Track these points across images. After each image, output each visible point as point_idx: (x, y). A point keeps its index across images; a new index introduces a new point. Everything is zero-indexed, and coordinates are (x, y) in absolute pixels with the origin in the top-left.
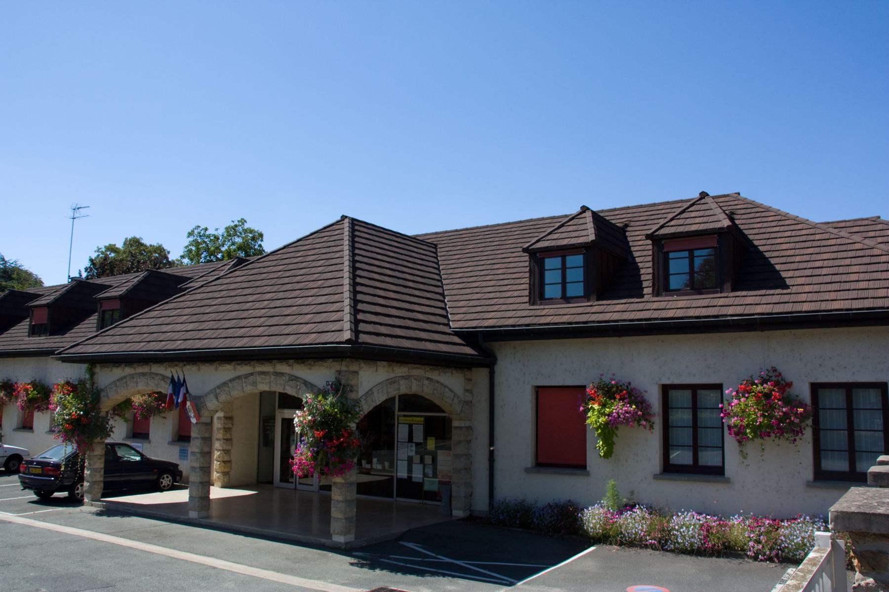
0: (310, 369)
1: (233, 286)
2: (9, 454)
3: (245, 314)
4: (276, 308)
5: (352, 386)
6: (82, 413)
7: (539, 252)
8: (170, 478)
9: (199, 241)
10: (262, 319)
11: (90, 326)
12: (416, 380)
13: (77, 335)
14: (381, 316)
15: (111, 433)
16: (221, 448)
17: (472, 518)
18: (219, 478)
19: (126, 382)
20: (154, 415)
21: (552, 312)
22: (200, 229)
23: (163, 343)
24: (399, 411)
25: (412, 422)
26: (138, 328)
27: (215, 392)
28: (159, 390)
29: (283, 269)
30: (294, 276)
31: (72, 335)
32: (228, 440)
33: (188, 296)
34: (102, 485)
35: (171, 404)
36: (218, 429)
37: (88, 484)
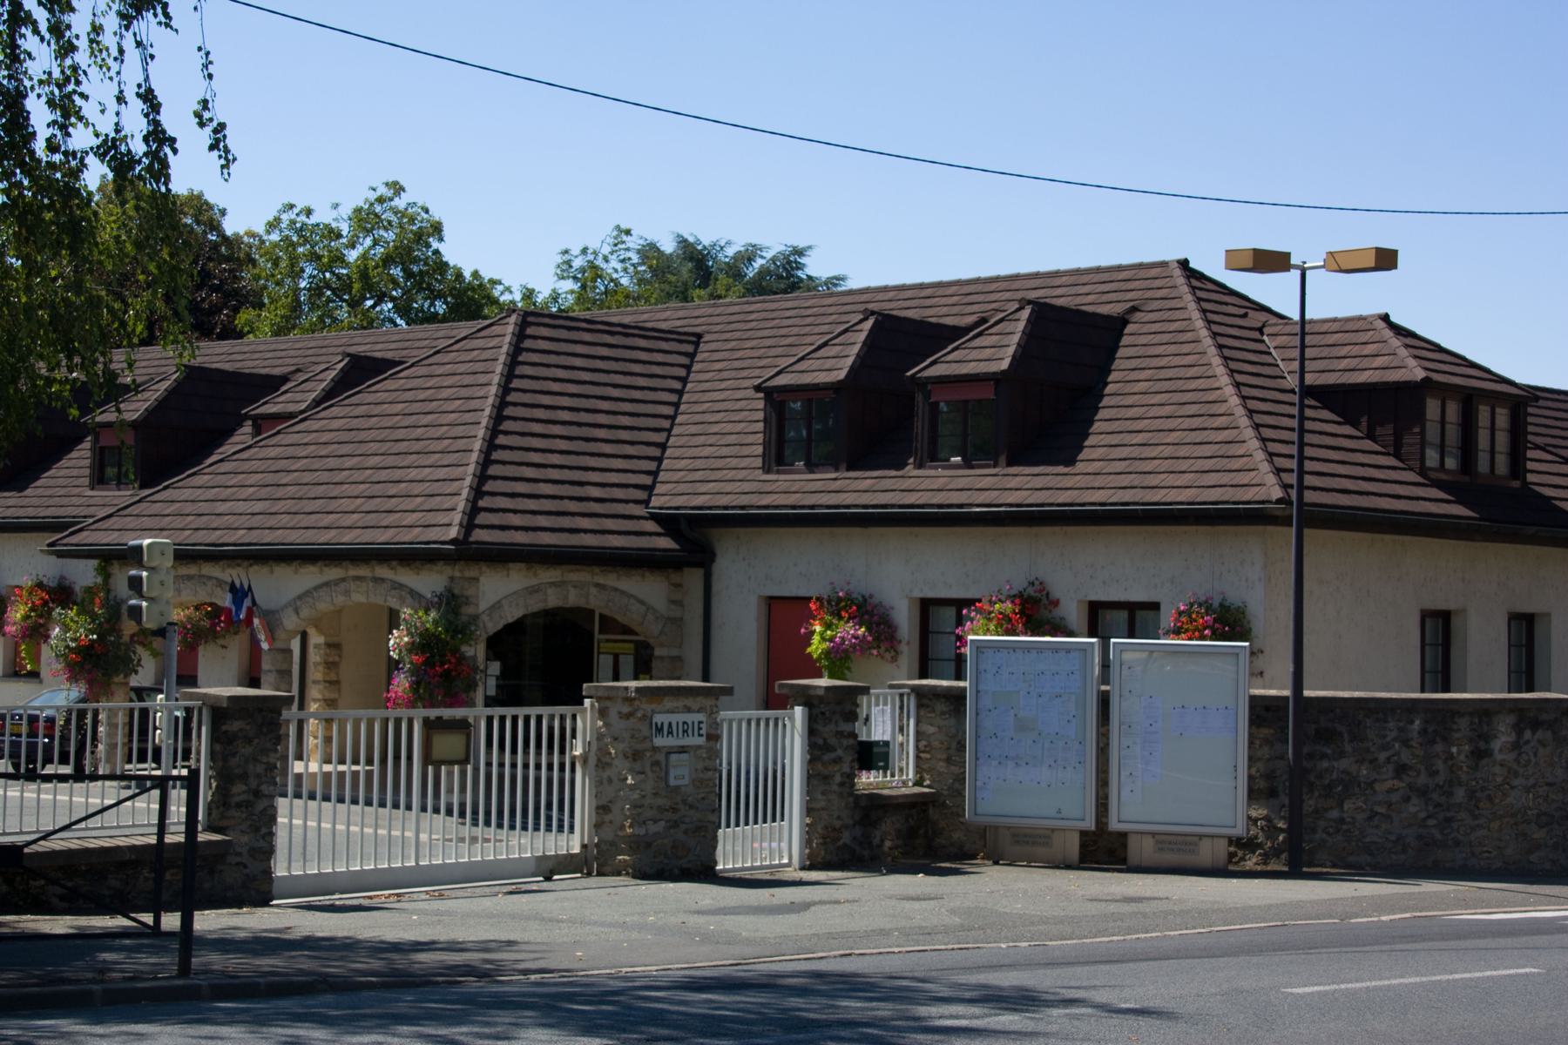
0: (418, 574)
1: (326, 437)
3: (336, 491)
4: (379, 482)
5: (467, 598)
6: (95, 637)
9: (295, 239)
10: (359, 501)
11: (75, 472)
12: (575, 587)
13: (49, 492)
14: (520, 499)
15: (140, 669)
16: (320, 697)
20: (206, 642)
22: (296, 211)
23: (218, 533)
24: (601, 632)
25: (617, 651)
26: (178, 505)
27: (295, 604)
28: (214, 600)
29: (403, 410)
30: (414, 427)
31: (39, 491)
32: (334, 684)
33: (256, 449)
35: (233, 625)
36: (316, 664)
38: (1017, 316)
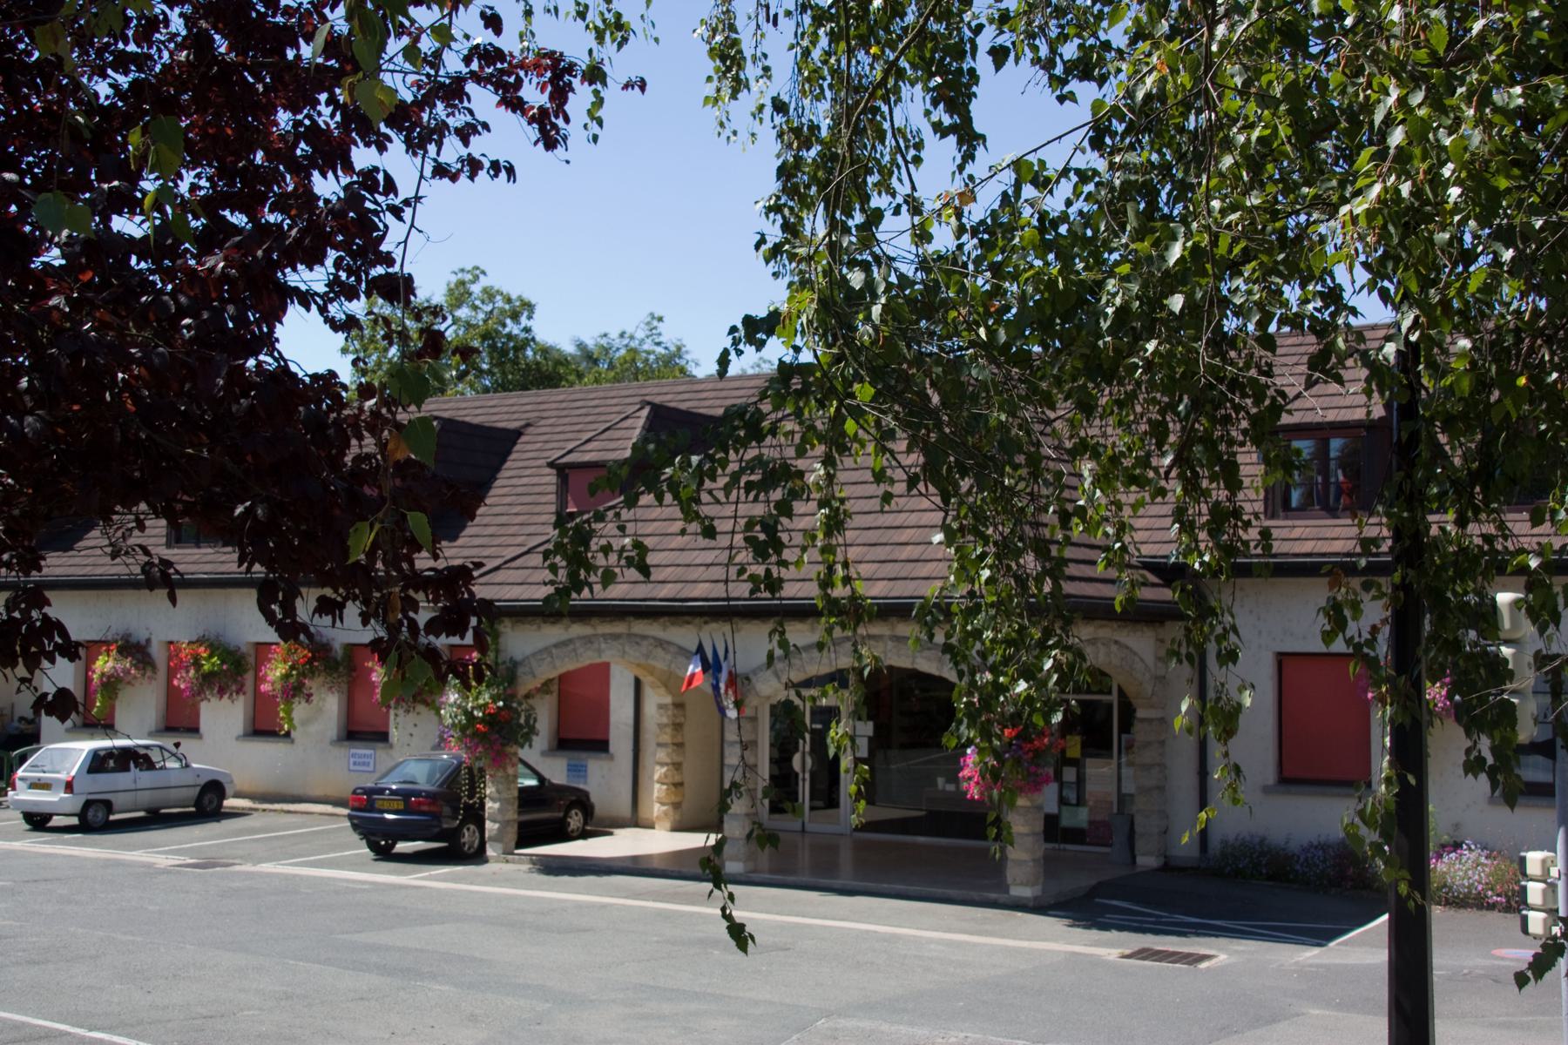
2: (203, 781)
7: (1283, 431)
8: (580, 814)
16: (668, 761)
17: (1169, 867)
18: (666, 813)
19: (575, 650)
21: (1307, 532)
34: (516, 826)
37: (497, 826)
38: (637, 414)
